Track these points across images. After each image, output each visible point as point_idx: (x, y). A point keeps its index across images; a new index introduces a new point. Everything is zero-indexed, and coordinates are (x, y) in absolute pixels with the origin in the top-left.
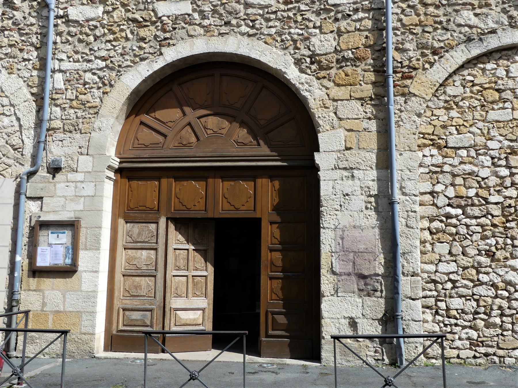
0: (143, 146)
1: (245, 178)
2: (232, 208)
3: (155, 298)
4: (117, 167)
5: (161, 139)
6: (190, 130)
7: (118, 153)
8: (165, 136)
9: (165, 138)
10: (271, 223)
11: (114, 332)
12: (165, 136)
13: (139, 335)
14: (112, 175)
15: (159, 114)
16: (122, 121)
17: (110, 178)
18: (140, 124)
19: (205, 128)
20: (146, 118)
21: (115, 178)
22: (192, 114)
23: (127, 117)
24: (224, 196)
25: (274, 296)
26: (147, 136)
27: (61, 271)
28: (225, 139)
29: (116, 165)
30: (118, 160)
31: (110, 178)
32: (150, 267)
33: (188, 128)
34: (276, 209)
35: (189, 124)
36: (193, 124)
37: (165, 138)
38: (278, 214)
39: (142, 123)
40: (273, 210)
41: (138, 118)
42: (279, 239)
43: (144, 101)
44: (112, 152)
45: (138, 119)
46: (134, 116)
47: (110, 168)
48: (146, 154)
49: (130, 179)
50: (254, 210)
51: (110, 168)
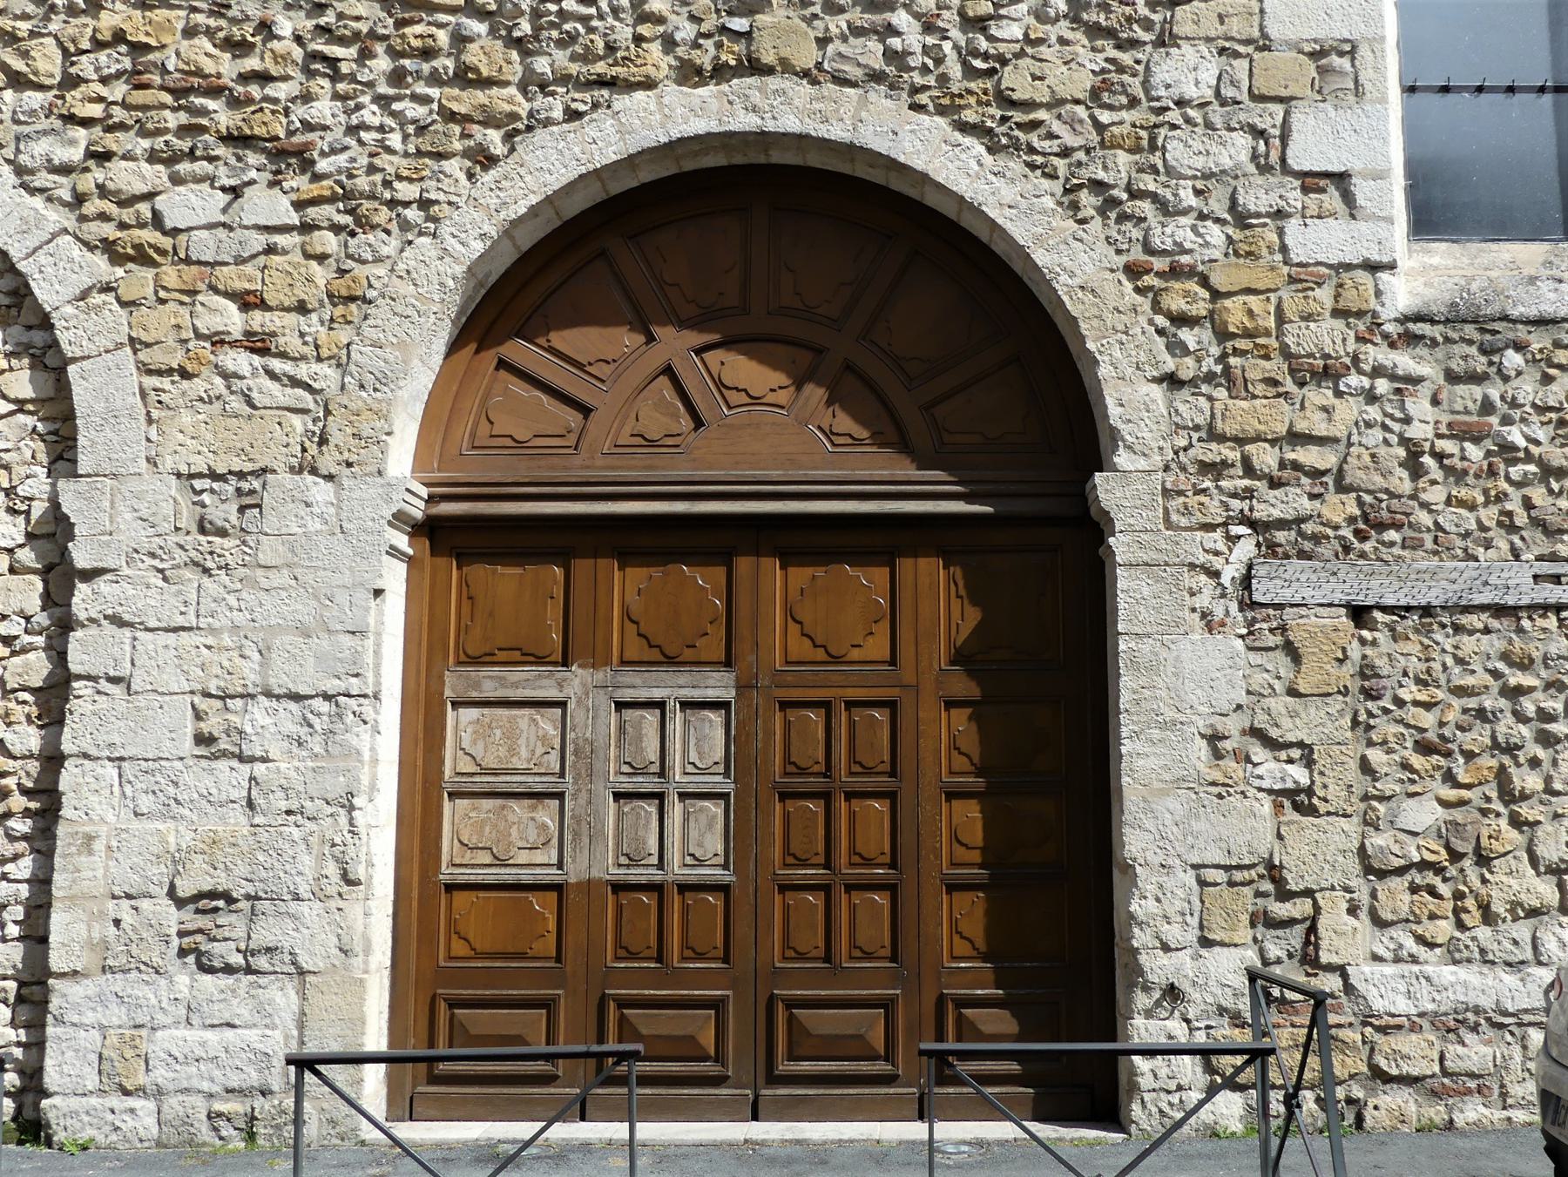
0: (509, 442)
1: (861, 557)
2: (820, 655)
3: (558, 959)
4: (419, 515)
5: (573, 418)
6: (669, 394)
7: (419, 463)
8: (586, 411)
9: (586, 418)
10: (950, 704)
11: (442, 964)
12: (586, 411)
13: (507, 994)
14: (402, 541)
15: (559, 339)
16: (437, 360)
17: (394, 552)
18: (497, 369)
19: (720, 385)
20: (519, 351)
21: (410, 552)
22: (675, 343)
23: (454, 347)
24: (627, 615)
25: (962, 947)
26: (524, 413)
27: (768, 340)
28: (775, 435)
29: (417, 511)
30: (424, 492)
31: (394, 552)
32: (539, 857)
33: (664, 381)
34: (961, 657)
35: (668, 371)
36: (679, 368)
37: (586, 418)
38: (970, 673)
39: (502, 364)
40: (952, 663)
41: (492, 352)
42: (976, 760)
43: (508, 306)
44: (400, 457)
45: (490, 357)
46: (473, 346)
47: (399, 519)
48: (522, 470)
49: (464, 557)
50: (893, 662)
51: (399, 519)
